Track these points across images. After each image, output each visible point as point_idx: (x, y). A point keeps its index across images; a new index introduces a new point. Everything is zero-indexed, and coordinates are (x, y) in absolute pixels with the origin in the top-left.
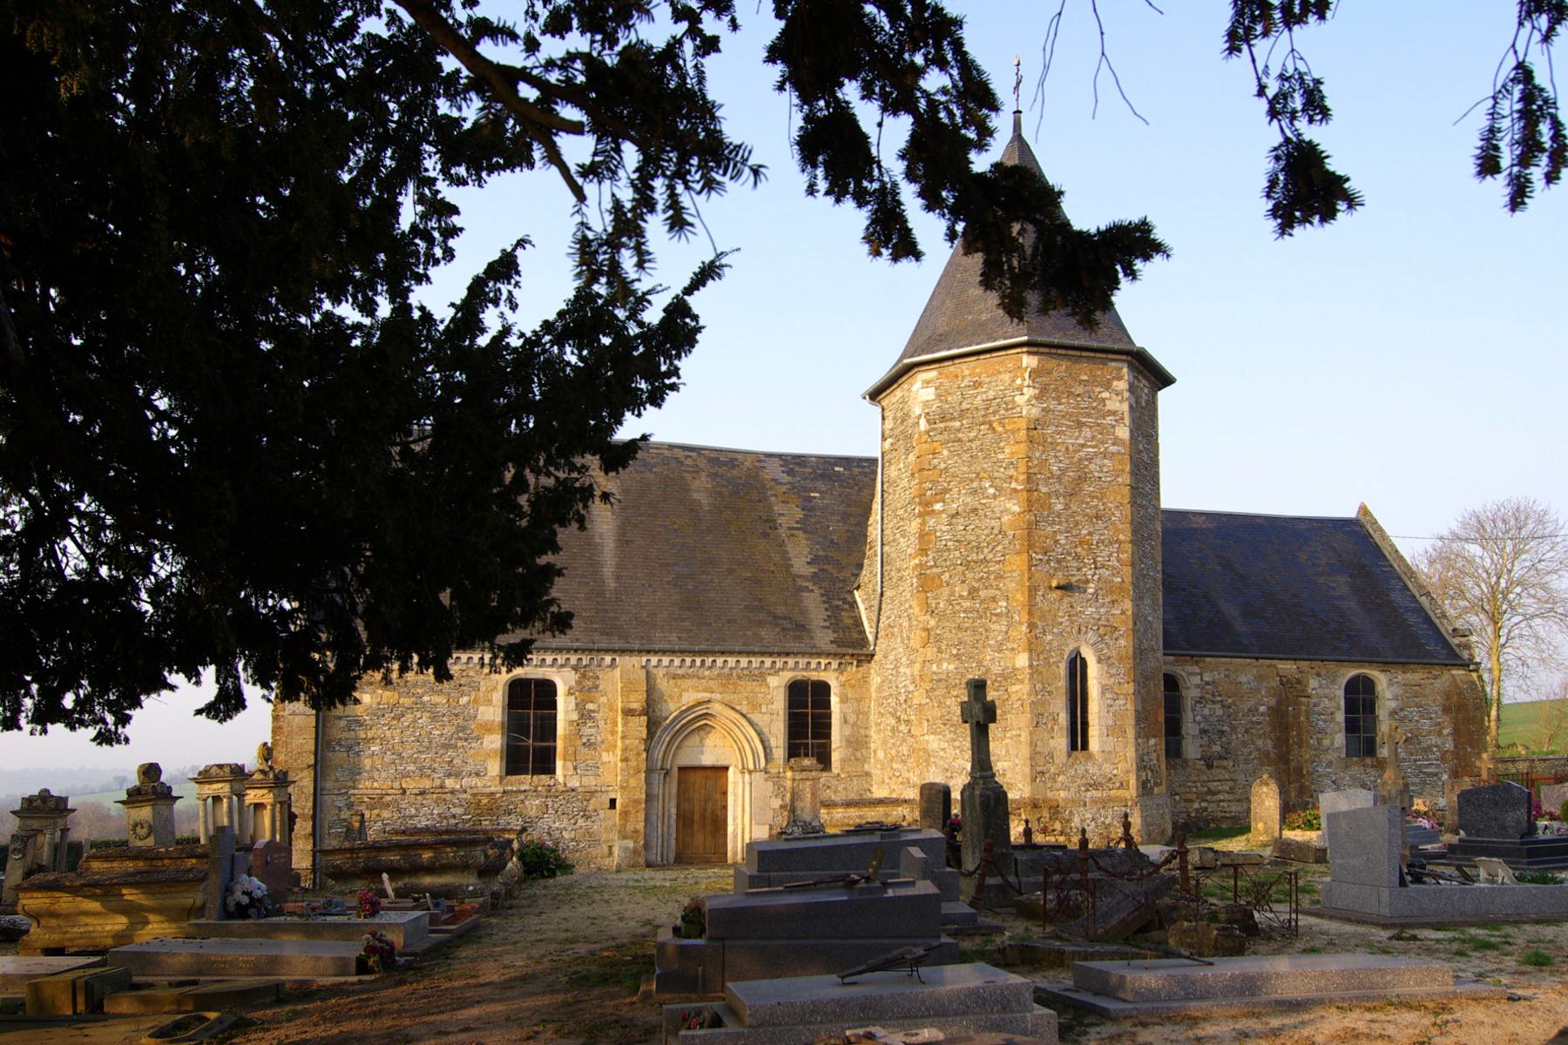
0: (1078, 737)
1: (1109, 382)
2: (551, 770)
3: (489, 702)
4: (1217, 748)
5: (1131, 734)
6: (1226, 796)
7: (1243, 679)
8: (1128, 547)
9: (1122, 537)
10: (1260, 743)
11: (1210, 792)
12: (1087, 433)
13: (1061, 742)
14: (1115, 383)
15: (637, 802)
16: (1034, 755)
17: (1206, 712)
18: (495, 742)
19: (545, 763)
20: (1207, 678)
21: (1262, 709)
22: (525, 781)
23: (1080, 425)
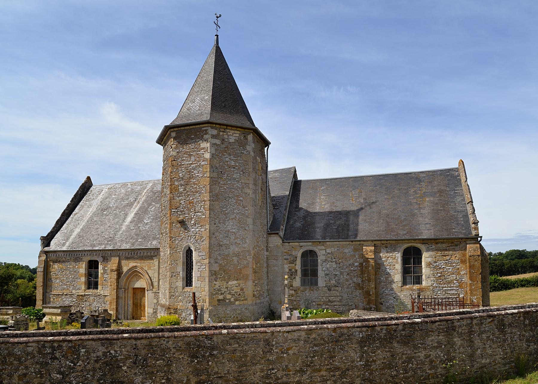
0: (188, 282)
1: (202, 136)
2: (97, 288)
3: (82, 268)
4: (333, 282)
5: (207, 280)
6: (338, 303)
7: (346, 251)
8: (208, 203)
9: (205, 199)
10: (355, 280)
11: (330, 301)
12: (193, 158)
13: (180, 284)
14: (205, 136)
15: (114, 299)
16: (171, 288)
17: (328, 266)
18: (83, 279)
19: (96, 287)
20: (328, 251)
21: (356, 264)
22: (91, 292)
23: (190, 155)
